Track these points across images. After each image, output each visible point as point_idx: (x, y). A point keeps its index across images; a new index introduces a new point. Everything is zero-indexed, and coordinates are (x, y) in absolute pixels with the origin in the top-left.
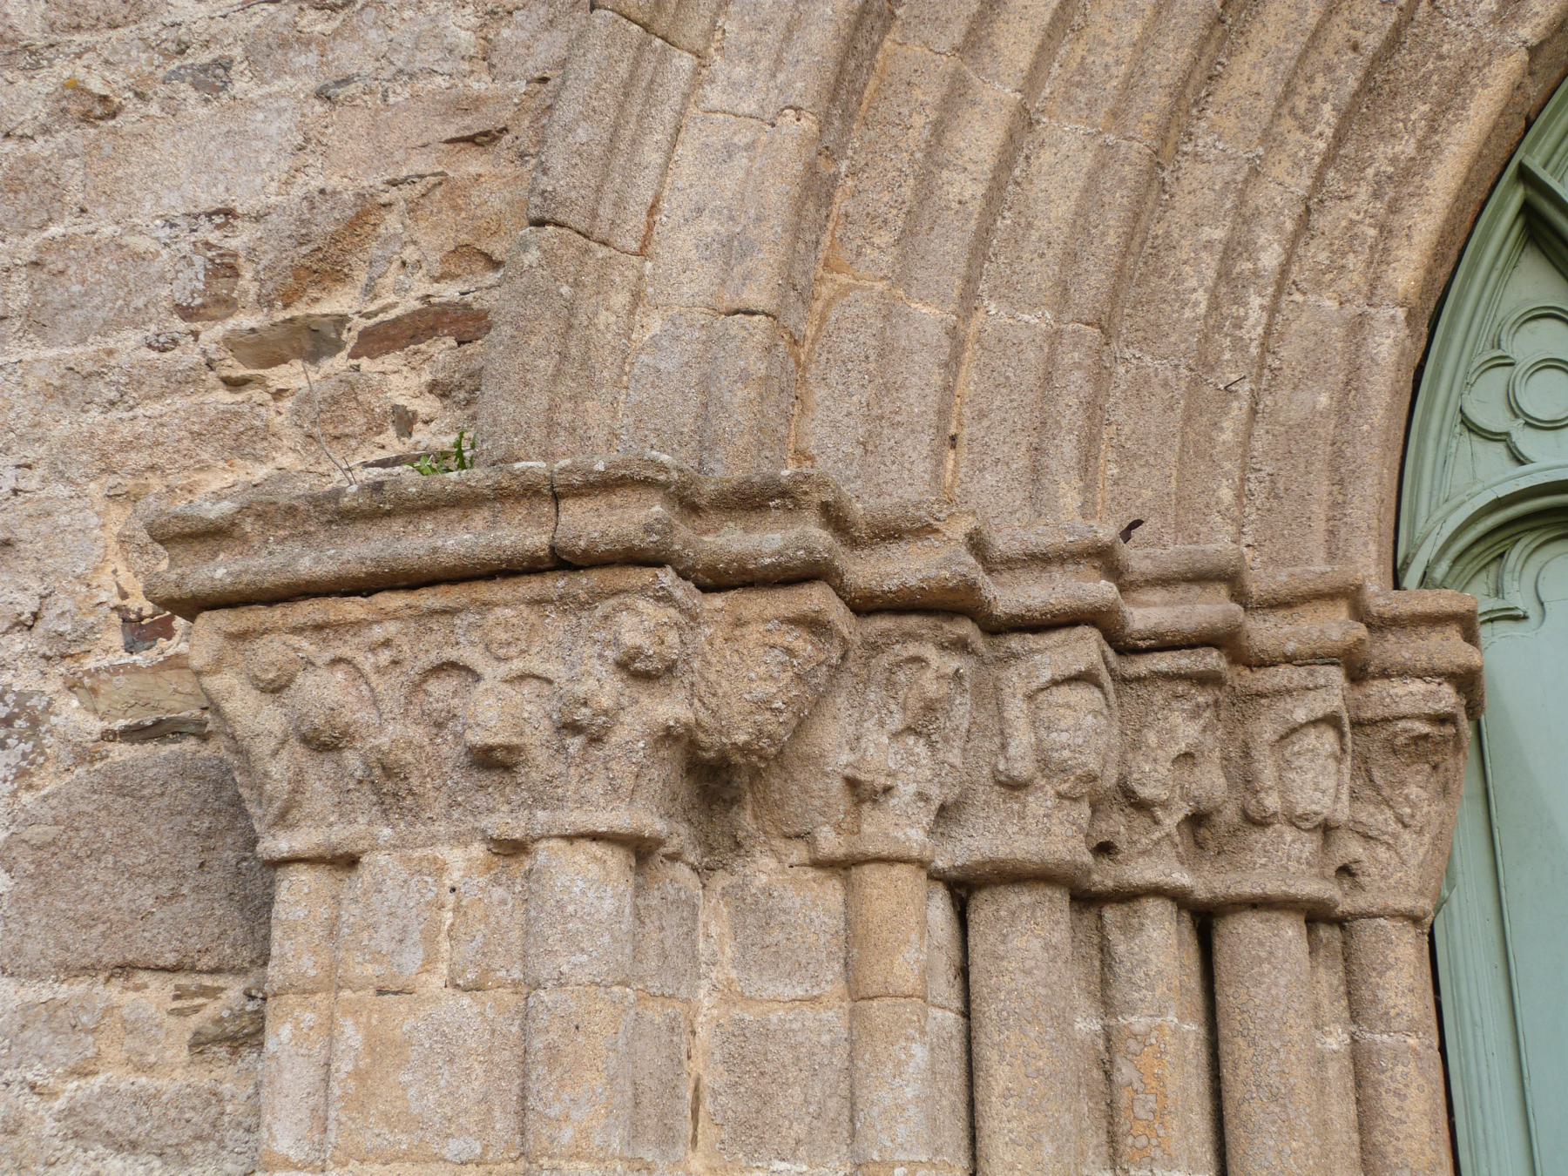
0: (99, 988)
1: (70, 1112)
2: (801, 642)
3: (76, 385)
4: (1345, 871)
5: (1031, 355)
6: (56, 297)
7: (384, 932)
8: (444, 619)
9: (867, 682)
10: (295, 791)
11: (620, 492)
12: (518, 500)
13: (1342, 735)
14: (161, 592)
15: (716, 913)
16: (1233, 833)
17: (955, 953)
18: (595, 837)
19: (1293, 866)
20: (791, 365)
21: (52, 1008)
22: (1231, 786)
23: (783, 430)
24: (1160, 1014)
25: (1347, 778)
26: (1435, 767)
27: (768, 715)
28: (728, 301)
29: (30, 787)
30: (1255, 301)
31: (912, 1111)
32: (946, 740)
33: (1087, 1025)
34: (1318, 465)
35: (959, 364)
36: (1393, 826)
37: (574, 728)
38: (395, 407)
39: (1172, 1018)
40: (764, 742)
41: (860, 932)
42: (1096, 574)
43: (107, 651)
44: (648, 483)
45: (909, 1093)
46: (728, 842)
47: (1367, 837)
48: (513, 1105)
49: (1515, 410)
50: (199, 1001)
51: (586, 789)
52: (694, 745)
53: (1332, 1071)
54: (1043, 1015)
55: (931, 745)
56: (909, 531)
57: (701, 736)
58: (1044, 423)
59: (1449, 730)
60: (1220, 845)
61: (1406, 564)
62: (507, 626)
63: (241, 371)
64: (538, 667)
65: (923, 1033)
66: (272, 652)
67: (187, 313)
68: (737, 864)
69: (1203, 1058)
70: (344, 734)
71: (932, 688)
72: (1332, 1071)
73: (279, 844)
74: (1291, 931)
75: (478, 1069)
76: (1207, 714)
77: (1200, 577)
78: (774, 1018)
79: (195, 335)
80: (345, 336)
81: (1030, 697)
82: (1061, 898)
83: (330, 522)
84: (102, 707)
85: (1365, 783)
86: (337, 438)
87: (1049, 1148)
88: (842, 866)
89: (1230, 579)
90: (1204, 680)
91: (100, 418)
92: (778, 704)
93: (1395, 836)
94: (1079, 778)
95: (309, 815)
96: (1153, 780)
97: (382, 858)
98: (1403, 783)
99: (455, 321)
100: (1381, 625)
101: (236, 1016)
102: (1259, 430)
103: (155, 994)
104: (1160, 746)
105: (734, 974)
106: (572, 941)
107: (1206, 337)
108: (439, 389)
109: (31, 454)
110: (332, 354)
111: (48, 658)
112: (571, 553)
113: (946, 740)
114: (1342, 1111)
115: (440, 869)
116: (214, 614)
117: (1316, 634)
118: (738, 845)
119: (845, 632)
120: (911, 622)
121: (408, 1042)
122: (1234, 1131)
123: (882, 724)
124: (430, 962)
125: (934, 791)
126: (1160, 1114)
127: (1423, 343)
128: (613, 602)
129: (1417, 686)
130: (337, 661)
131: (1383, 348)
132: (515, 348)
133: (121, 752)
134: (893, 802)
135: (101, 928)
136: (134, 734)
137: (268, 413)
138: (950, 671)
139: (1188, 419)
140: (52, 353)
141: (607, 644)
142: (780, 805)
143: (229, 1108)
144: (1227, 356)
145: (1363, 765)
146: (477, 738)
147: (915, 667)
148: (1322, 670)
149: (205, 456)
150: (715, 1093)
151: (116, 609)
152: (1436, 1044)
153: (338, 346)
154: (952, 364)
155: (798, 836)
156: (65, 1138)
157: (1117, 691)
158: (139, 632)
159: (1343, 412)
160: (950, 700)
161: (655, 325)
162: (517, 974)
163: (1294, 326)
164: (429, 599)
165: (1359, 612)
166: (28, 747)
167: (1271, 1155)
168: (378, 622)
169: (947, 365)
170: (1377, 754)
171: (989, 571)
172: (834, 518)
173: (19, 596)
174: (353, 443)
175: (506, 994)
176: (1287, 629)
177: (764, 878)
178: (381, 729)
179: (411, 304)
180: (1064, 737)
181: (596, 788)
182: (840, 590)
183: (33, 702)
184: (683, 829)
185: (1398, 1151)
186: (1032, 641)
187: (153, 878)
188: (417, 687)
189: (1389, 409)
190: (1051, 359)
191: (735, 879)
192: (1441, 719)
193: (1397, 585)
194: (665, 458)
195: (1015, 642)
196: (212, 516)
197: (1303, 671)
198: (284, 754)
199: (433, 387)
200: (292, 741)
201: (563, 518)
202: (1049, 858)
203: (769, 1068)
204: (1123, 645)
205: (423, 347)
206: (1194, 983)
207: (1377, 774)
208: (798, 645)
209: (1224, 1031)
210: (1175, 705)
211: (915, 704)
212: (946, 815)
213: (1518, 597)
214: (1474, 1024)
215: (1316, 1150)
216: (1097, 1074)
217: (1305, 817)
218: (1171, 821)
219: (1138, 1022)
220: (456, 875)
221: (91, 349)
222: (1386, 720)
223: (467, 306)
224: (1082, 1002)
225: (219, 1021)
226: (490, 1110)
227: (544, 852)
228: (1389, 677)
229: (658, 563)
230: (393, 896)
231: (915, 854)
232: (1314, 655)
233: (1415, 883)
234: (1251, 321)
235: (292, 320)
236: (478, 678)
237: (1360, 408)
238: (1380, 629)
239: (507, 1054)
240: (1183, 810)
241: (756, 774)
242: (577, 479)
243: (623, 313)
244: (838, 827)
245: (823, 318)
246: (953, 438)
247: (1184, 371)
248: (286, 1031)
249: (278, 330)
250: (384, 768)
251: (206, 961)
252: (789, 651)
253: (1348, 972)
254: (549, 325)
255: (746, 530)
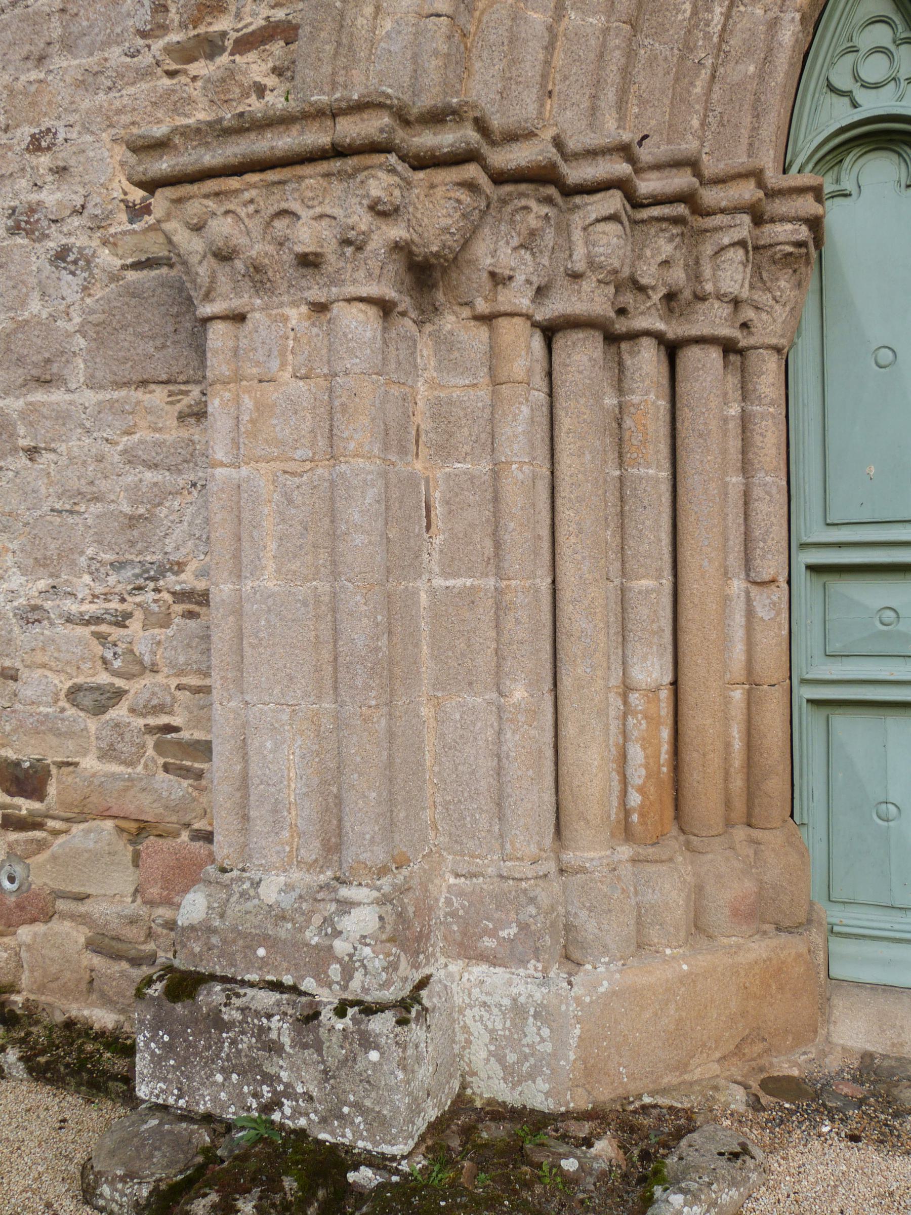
0: (132, 392)
1: (125, 452)
2: (463, 195)
3: (91, 79)
4: (745, 326)
5: (593, 42)
6: (75, 29)
7: (260, 351)
8: (280, 187)
9: (500, 221)
10: (212, 282)
11: (367, 111)
12: (314, 119)
13: (747, 252)
14: (136, 178)
15: (426, 345)
16: (689, 304)
17: (545, 365)
18: (361, 300)
19: (717, 321)
20: (462, 48)
21: (112, 402)
22: (689, 279)
23: (458, 86)
24: (646, 394)
25: (748, 276)
26: (795, 271)
27: (448, 236)
28: (427, 9)
29: (89, 295)
30: (718, 10)
31: (521, 437)
32: (541, 252)
33: (610, 401)
34: (746, 107)
35: (554, 49)
36: (771, 302)
37: (347, 242)
38: (255, 83)
39: (652, 396)
40: (447, 251)
41: (497, 351)
42: (621, 160)
43: (120, 224)
44: (380, 106)
45: (520, 429)
46: (431, 308)
47: (757, 308)
48: (327, 434)
49: (857, 78)
50: (180, 397)
51: (356, 275)
52: (411, 254)
53: (731, 425)
54: (588, 394)
55: (533, 254)
56: (522, 136)
57: (414, 248)
58: (598, 82)
59: (803, 250)
60: (681, 311)
61: (790, 165)
62: (312, 189)
63: (174, 67)
64: (328, 210)
65: (527, 400)
66: (194, 208)
67: (144, 34)
68: (436, 319)
69: (668, 418)
70: (234, 251)
71: (533, 221)
72: (731, 425)
73: (207, 310)
74: (714, 355)
75: (309, 416)
76: (677, 239)
77: (677, 164)
78: (455, 395)
79: (149, 47)
80: (226, 43)
81: (585, 229)
82: (598, 336)
83: (218, 136)
84: (120, 253)
85: (758, 279)
86: (226, 101)
87: (588, 457)
88: (487, 319)
89: (692, 164)
90: (677, 221)
91: (104, 98)
92: (453, 230)
93: (772, 307)
94: (609, 272)
95: (220, 295)
96: (648, 274)
97: (257, 315)
98: (777, 279)
99: (283, 31)
100: (772, 194)
101: (197, 404)
102: (716, 88)
103: (158, 396)
104: (652, 257)
105: (435, 375)
106: (351, 352)
107: (689, 31)
108: (278, 71)
109: (72, 118)
110: (220, 54)
111: (91, 229)
112: (343, 146)
113: (541, 252)
114: (734, 444)
115: (286, 319)
116: (164, 189)
117: (737, 196)
118: (437, 309)
119: (488, 191)
120: (523, 187)
121: (275, 405)
122: (681, 452)
123: (508, 243)
124: (283, 365)
125: (534, 279)
126: (644, 442)
127: (810, 38)
128: (365, 173)
129: (789, 227)
130: (227, 212)
131: (787, 37)
132: (312, 38)
133: (132, 276)
134: (513, 284)
135: (130, 363)
136: (137, 266)
137: (190, 90)
138: (543, 213)
139: (677, 80)
140: (77, 62)
141: (363, 197)
142: (456, 287)
143: (198, 447)
144: (700, 43)
145: (758, 270)
146: (299, 249)
147: (525, 212)
148: (739, 216)
149: (159, 115)
150: (427, 432)
151: (122, 201)
152: (784, 413)
153: (223, 49)
154: (550, 48)
155: (466, 304)
156: (125, 464)
157: (631, 228)
158: (137, 212)
159: (761, 76)
160: (543, 230)
161: (388, 25)
162: (326, 371)
163: (739, 26)
164: (272, 176)
165: (761, 184)
166: (86, 275)
167: (697, 463)
168: (247, 190)
169: (546, 48)
170: (766, 264)
171: (566, 161)
172: (481, 126)
173: (74, 197)
174: (235, 104)
175: (321, 381)
176: (722, 194)
177: (449, 326)
178: (252, 247)
179: (260, 22)
180: (601, 250)
181: (361, 274)
182: (485, 168)
183: (87, 251)
184: (407, 299)
185: (759, 462)
186: (587, 199)
187: (153, 338)
188: (269, 224)
189: (787, 73)
190: (604, 45)
191: (435, 327)
192: (800, 244)
193: (785, 171)
194: (389, 91)
195: (578, 200)
196: (158, 135)
197: (729, 217)
198: (205, 263)
199: (274, 70)
200: (209, 256)
201: (338, 127)
202: (592, 314)
203: (452, 419)
204: (635, 202)
205: (267, 47)
206: (665, 382)
207: (765, 275)
208: (463, 197)
209: (678, 405)
210: (661, 234)
211: (525, 232)
212: (541, 292)
213: (848, 184)
214: (804, 405)
215: (719, 460)
216: (614, 425)
217: (725, 295)
218: (656, 297)
219: (635, 399)
220: (294, 322)
221: (96, 59)
222: (771, 246)
223: (289, 22)
224: (609, 390)
225: (190, 406)
226: (315, 436)
227: (336, 308)
228: (774, 222)
229: (388, 151)
230: (264, 334)
231: (524, 311)
232: (735, 208)
233: (780, 332)
234: (715, 22)
235: (198, 35)
236: (298, 218)
237: (771, 73)
238: (772, 196)
239: (322, 410)
240: (662, 291)
241: (445, 271)
242: (344, 105)
243: (370, 18)
244: (486, 299)
245: (480, 21)
246: (550, 92)
247: (676, 51)
248: (217, 402)
249: (192, 41)
250: (254, 268)
251: (182, 378)
252: (458, 201)
253: (743, 377)
254: (330, 25)
255: (435, 134)
